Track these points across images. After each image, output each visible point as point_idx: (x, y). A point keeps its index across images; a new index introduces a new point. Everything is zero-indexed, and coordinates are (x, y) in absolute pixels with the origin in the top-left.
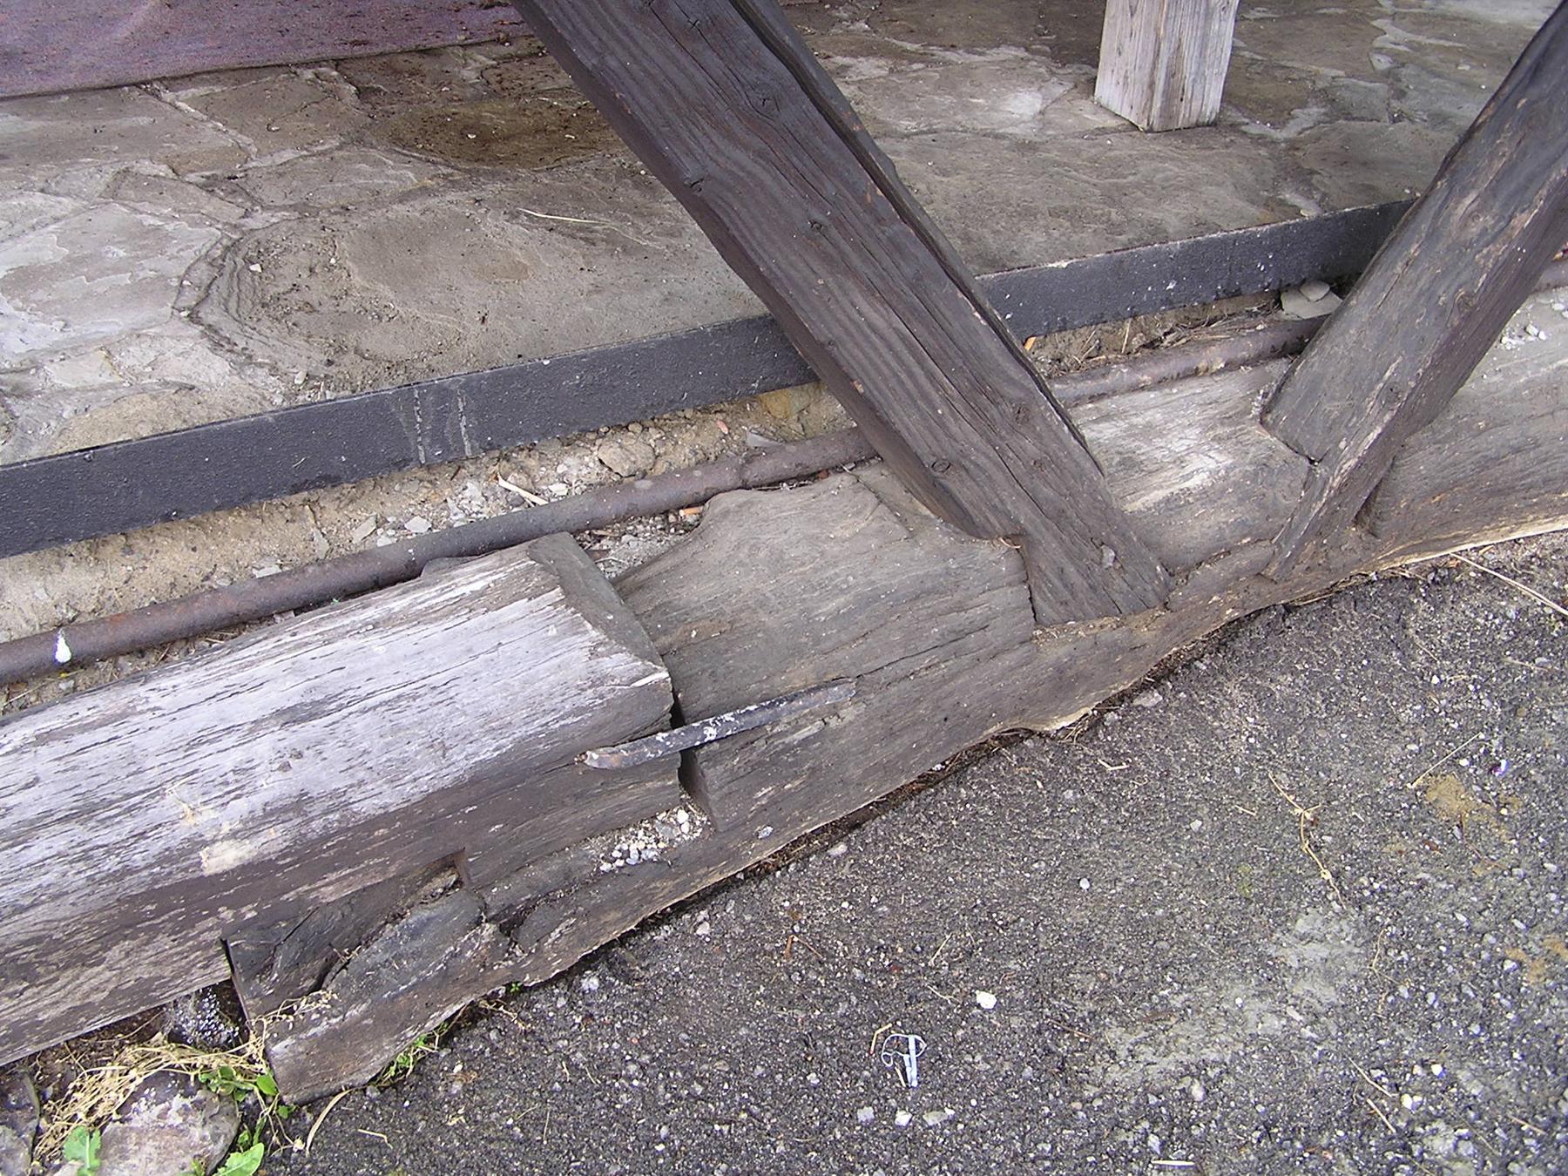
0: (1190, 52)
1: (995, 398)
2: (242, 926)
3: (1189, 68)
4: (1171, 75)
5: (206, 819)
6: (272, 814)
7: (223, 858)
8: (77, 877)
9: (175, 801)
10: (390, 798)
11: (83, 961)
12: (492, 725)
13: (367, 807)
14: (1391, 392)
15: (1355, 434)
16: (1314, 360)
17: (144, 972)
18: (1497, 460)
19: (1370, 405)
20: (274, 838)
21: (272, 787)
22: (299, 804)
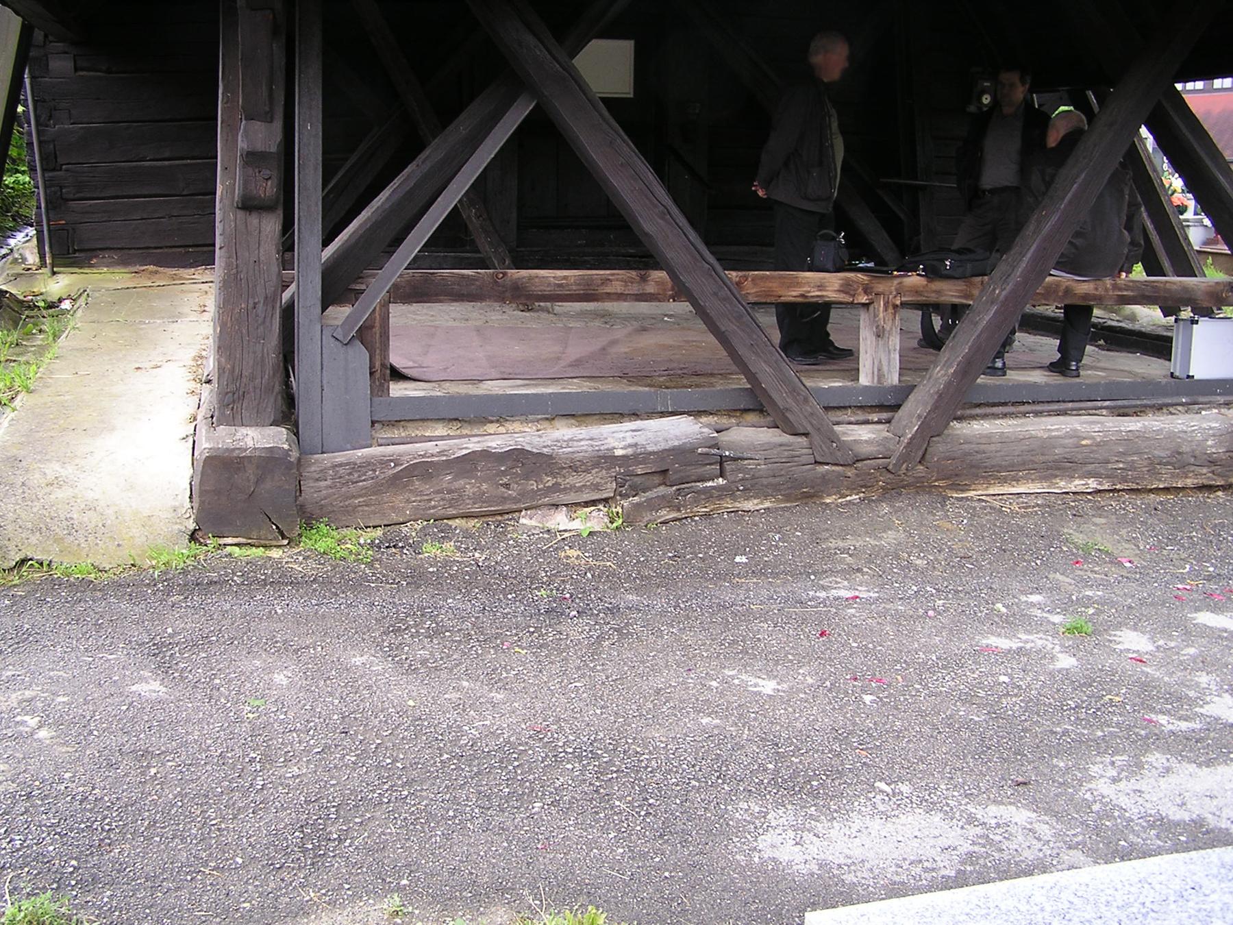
0: (885, 363)
1: (799, 394)
2: (620, 473)
3: (885, 368)
4: (879, 370)
5: (616, 444)
6: (630, 446)
7: (619, 453)
8: (590, 449)
9: (610, 440)
10: (655, 449)
11: (587, 471)
12: (677, 438)
13: (650, 449)
14: (919, 416)
15: (911, 428)
16: (900, 412)
17: (598, 480)
18: (970, 454)
19: (914, 420)
20: (630, 451)
21: (630, 441)
22: (636, 445)
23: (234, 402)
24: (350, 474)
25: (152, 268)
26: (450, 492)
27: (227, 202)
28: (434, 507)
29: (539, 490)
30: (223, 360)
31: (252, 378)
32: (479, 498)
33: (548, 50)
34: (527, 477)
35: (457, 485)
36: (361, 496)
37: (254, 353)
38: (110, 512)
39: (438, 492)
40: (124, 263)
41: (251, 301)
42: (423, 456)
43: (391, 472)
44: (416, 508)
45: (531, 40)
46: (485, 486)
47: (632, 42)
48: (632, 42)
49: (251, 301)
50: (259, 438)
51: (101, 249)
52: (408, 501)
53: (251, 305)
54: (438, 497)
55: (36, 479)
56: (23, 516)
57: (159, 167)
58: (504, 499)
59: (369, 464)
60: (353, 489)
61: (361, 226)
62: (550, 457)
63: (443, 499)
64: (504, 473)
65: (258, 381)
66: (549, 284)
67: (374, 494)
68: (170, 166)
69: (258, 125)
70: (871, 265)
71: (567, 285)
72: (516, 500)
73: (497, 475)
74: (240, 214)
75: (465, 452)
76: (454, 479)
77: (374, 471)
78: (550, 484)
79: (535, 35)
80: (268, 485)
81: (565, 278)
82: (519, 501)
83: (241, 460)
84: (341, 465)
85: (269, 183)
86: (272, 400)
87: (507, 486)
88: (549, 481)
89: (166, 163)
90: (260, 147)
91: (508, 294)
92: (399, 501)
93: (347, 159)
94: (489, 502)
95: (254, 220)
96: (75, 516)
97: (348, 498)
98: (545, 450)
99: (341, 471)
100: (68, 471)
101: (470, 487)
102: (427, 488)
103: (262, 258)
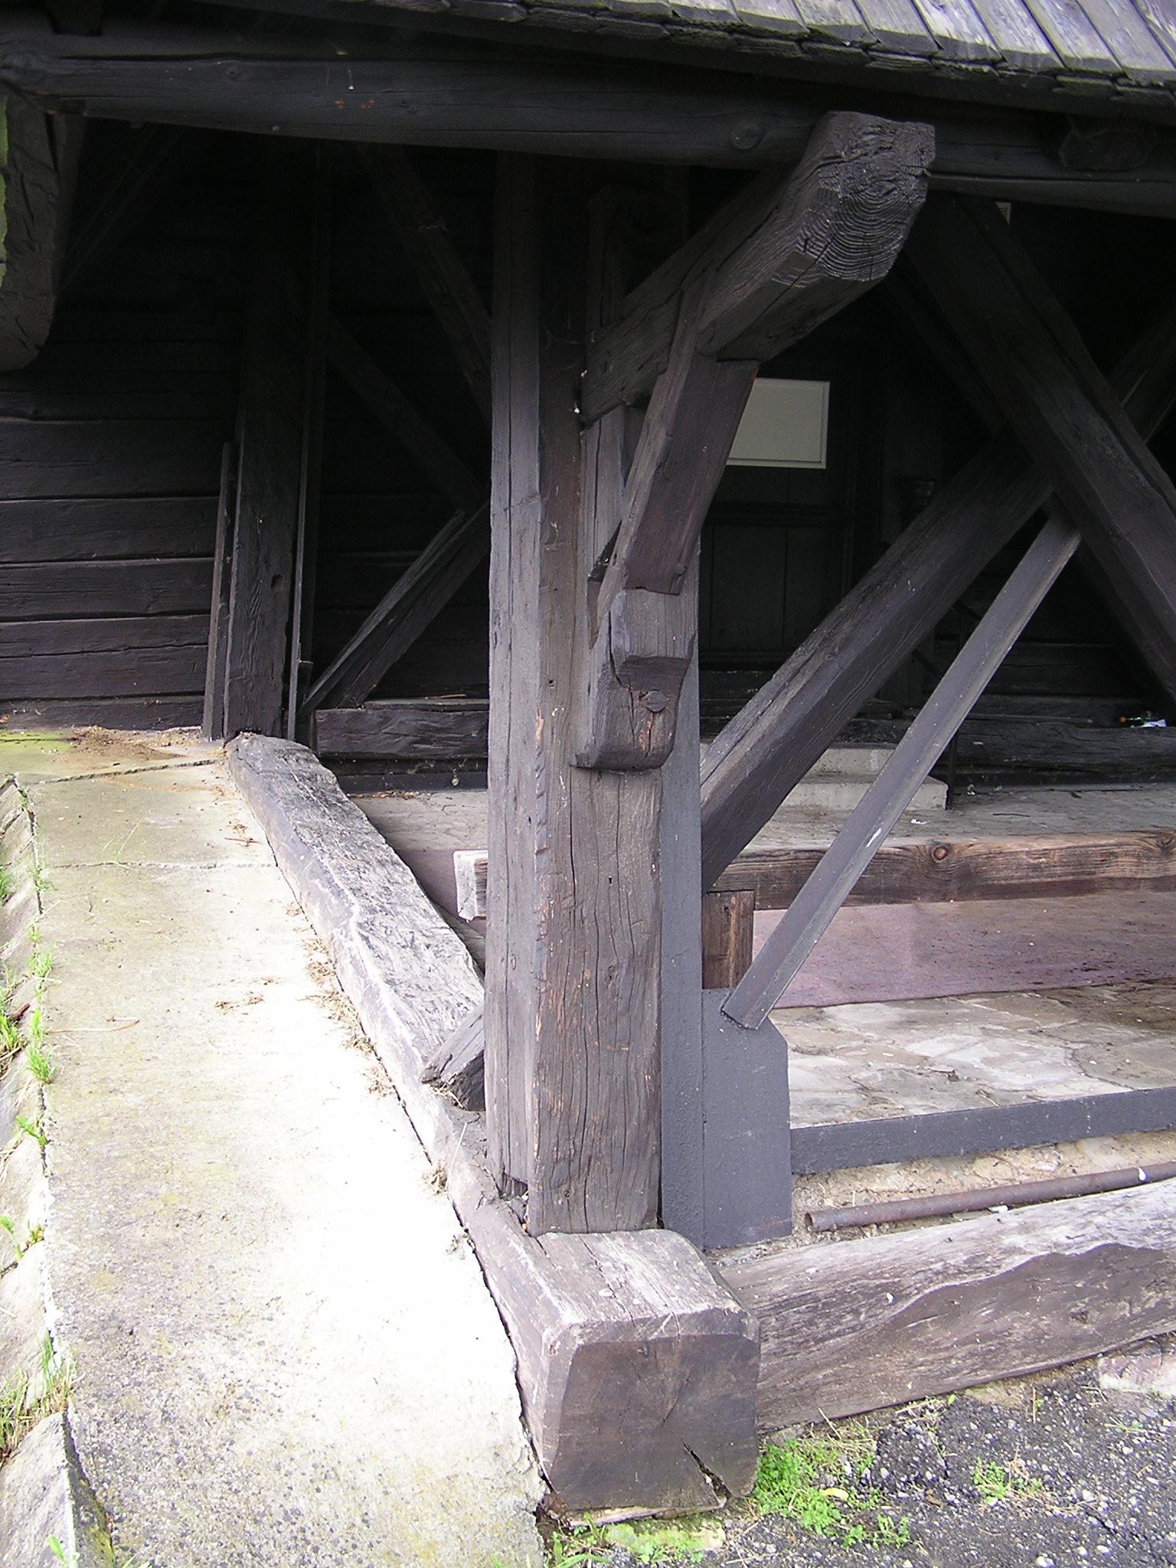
23: (570, 1178)
24: (810, 1323)
25: (95, 730)
26: (986, 1337)
27: (553, 754)
28: (955, 1371)
29: (1134, 1317)
30: (548, 1092)
31: (606, 1127)
32: (1034, 1344)
33: (1122, 442)
34: (1115, 1295)
35: (998, 1324)
36: (828, 1365)
37: (610, 1073)
38: (366, 1478)
39: (962, 1343)
40: (52, 721)
41: (603, 964)
42: (944, 1273)
43: (889, 1314)
44: (923, 1377)
45: (1095, 424)
46: (1046, 1320)
47: (827, 385)
48: (827, 385)
49: (603, 964)
50: (651, 1280)
51: (13, 700)
52: (911, 1365)
53: (602, 974)
54: (962, 1352)
55: (190, 1401)
56: (195, 1524)
57: (110, 570)
58: (1076, 1341)
59: (844, 1297)
60: (816, 1353)
61: (731, 772)
62: (1158, 1254)
63: (972, 1354)
64: (1080, 1294)
65: (618, 1132)
66: (1019, 866)
67: (855, 1357)
68: (129, 567)
69: (651, 602)
70: (1161, 723)
71: (1048, 866)
72: (1093, 1340)
73: (1068, 1298)
74: (580, 780)
75: (1019, 1260)
76: (996, 1315)
77: (856, 1313)
78: (1152, 1304)
79: (1104, 415)
80: (704, 1395)
81: (1045, 853)
82: (1100, 1341)
83: (650, 1349)
84: (788, 1304)
85: (659, 719)
86: (644, 1168)
87: (1082, 1317)
88: (1152, 1298)
89: (123, 563)
90: (654, 646)
91: (953, 886)
92: (894, 1364)
93: (416, 557)
94: (1047, 1351)
95: (606, 792)
96: (302, 1505)
97: (804, 1372)
98: (1150, 1241)
99: (793, 1316)
100: (248, 1366)
101: (1019, 1325)
102: (947, 1336)
103: (625, 872)
